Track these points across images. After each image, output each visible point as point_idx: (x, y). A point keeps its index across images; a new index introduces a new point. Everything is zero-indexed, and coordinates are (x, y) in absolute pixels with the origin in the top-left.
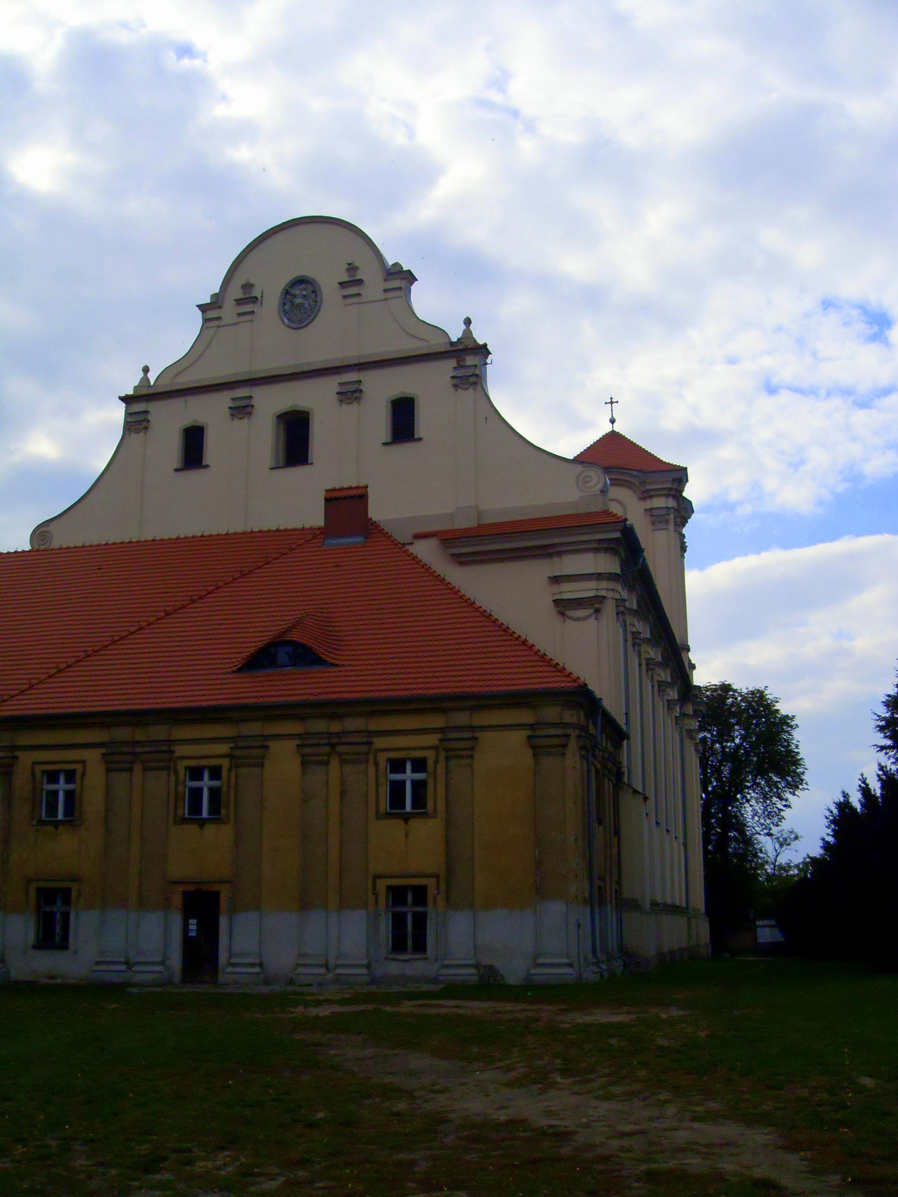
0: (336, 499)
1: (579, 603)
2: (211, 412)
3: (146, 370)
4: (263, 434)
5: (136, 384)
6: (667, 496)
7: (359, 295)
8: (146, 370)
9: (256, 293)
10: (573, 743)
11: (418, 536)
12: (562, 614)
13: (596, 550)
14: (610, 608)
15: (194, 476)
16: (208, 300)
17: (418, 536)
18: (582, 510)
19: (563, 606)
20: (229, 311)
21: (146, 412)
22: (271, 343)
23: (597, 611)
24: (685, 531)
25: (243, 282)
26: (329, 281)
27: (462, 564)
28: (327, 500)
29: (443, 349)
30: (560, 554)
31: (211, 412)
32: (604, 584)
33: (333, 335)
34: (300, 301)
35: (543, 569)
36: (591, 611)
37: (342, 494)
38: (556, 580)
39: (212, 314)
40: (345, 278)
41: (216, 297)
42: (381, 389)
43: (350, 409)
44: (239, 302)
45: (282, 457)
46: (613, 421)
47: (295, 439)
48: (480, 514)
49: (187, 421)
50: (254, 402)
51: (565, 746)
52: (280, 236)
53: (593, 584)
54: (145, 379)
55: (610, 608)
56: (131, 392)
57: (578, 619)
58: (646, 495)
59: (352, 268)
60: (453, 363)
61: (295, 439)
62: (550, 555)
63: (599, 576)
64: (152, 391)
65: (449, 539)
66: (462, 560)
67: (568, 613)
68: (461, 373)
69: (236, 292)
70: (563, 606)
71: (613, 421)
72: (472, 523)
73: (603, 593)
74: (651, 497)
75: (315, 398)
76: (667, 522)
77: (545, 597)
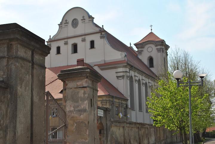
0: (79, 61)
1: (120, 77)
2: (61, 44)
3: (50, 36)
4: (70, 47)
5: (49, 39)
6: (160, 46)
7: (84, 22)
8: (50, 36)
9: (68, 22)
10: (108, 103)
11: (95, 65)
12: (118, 78)
13: (123, 67)
14: (125, 77)
15: (59, 55)
16: (60, 23)
17: (95, 65)
18: (121, 60)
19: (118, 77)
20: (63, 25)
21: (50, 44)
22: (70, 31)
23: (123, 78)
24: (168, 51)
25: (65, 20)
26: (79, 19)
27: (102, 70)
28: (77, 61)
29: (98, 31)
30: (117, 68)
31: (61, 44)
32: (124, 73)
33: (81, 29)
34: (75, 23)
35: (114, 71)
36: (122, 78)
37: (81, 60)
38: (117, 73)
39: (60, 26)
40: (82, 19)
41: (61, 22)
42: (89, 39)
43: (84, 43)
44: (65, 23)
45: (72, 52)
46: (151, 30)
47: (75, 48)
48: (105, 61)
49: (57, 46)
50: (68, 42)
51: (106, 104)
52: (67, 14)
53: (122, 73)
54: (50, 38)
55: (125, 77)
56: (48, 40)
57: (120, 79)
58: (156, 46)
59: (83, 17)
60: (100, 34)
61: (75, 48)
62: (116, 68)
63: (123, 72)
64: (51, 40)
65: (99, 66)
66: (102, 69)
67: (119, 78)
68: (102, 36)
69: (64, 22)
70: (118, 77)
71: (151, 30)
72: (103, 63)
73: (124, 75)
74: (157, 46)
75: (78, 41)
76: (161, 51)
77: (115, 75)
